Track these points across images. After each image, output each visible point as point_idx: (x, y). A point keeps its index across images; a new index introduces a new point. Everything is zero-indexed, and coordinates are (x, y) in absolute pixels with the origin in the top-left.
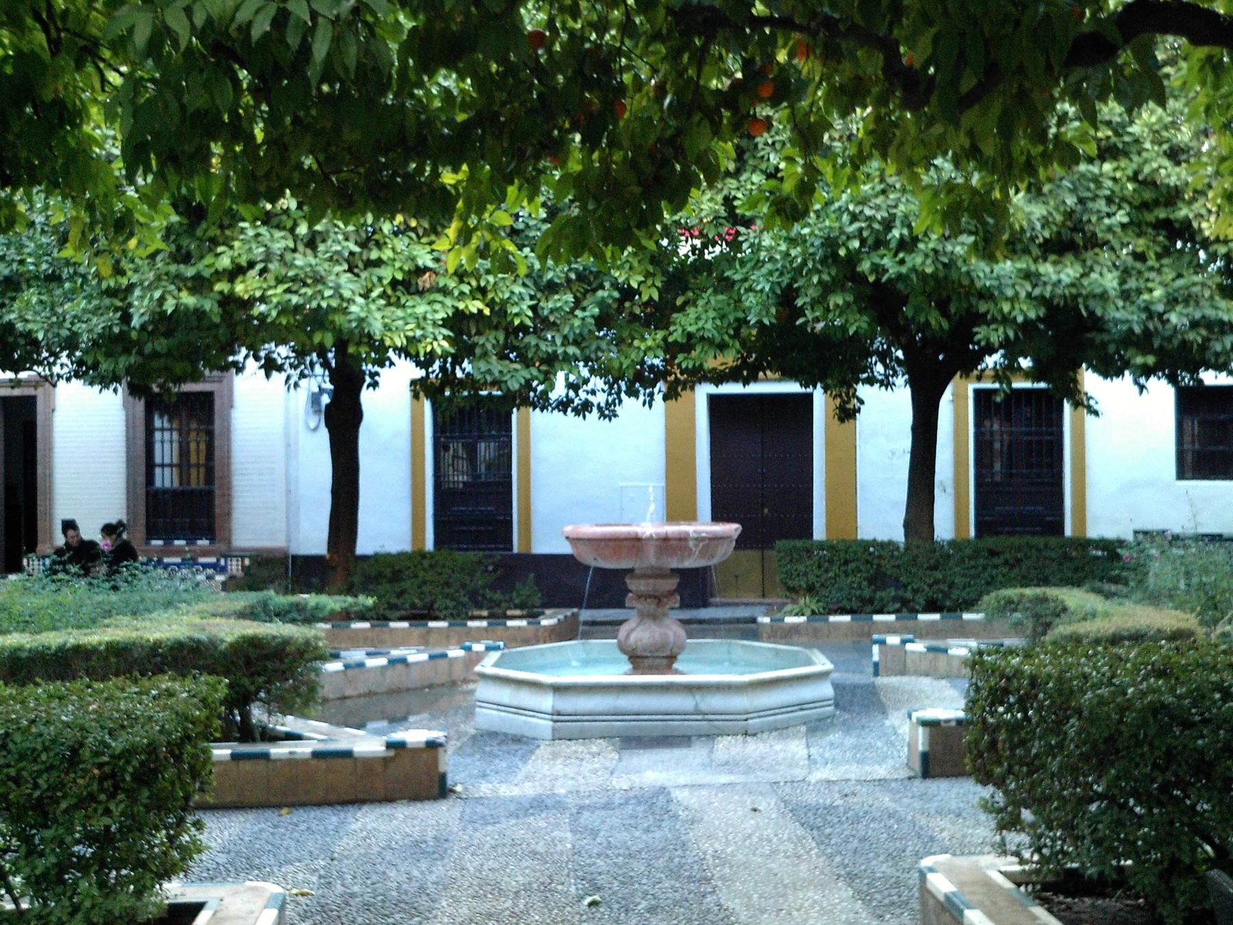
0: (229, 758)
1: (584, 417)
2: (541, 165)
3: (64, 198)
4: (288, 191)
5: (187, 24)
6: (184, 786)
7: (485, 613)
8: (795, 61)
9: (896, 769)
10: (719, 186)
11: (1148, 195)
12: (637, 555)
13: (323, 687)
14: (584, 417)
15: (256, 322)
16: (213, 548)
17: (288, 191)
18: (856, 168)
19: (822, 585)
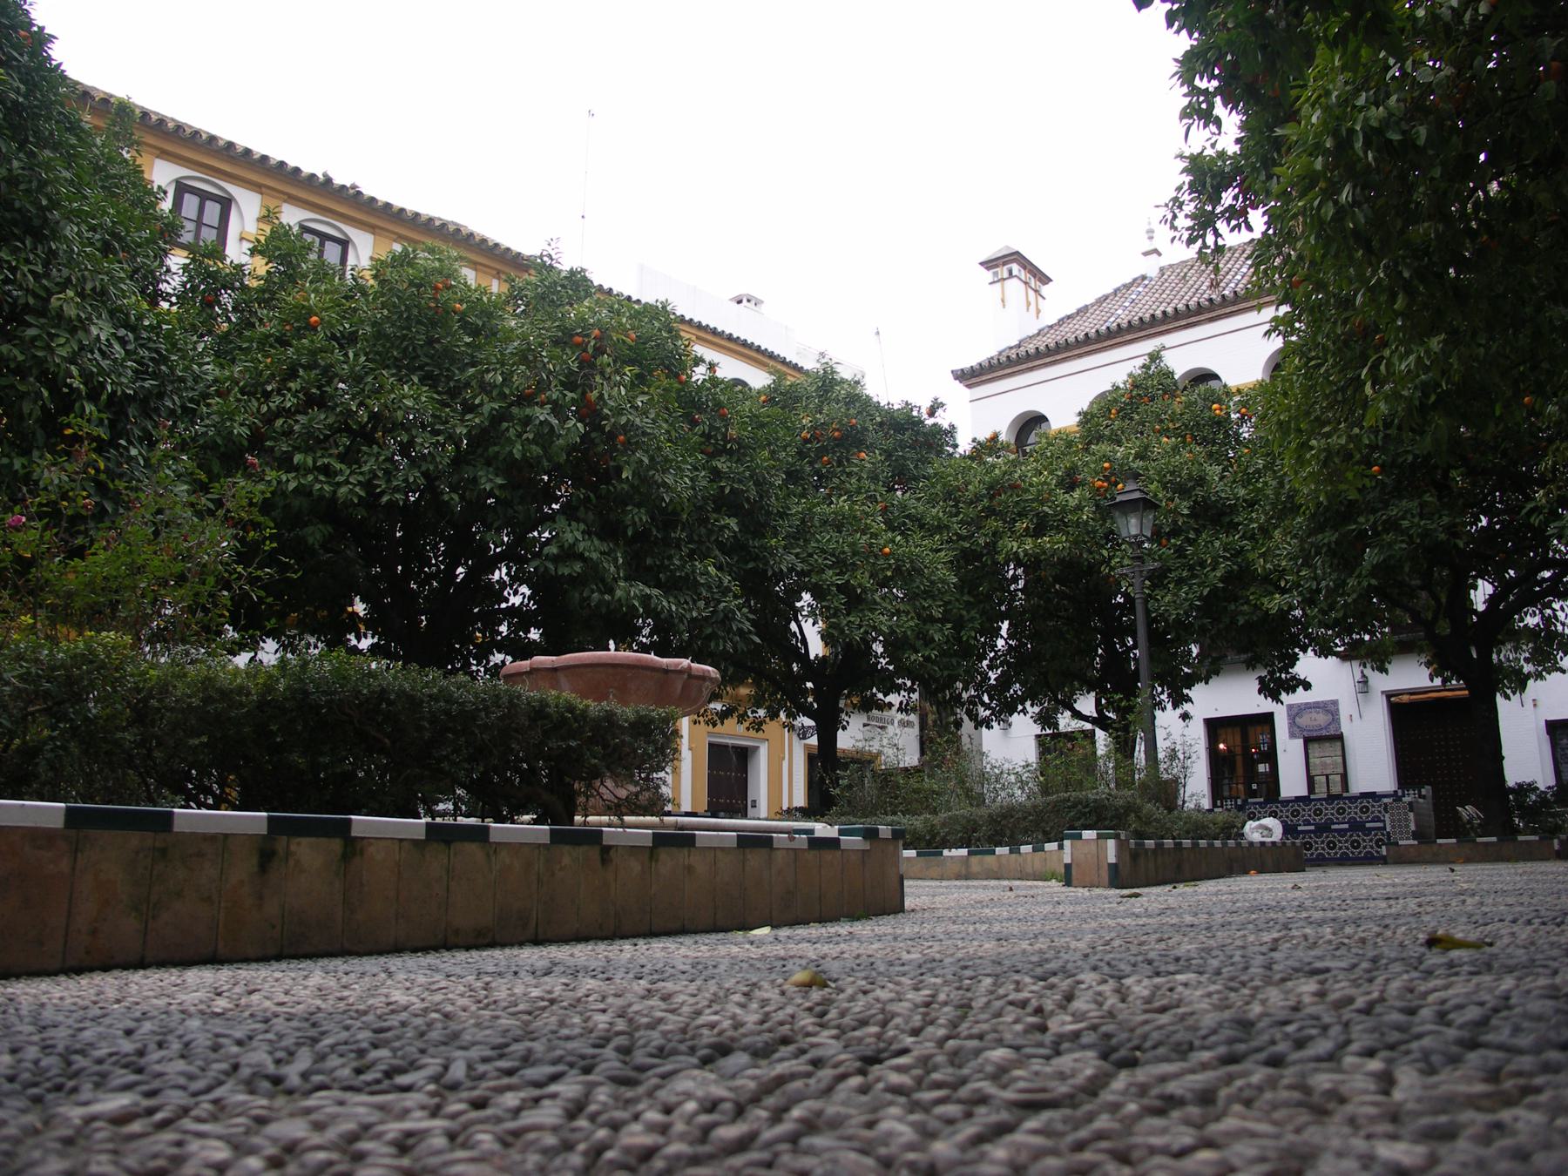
0: (58, 823)
1: (1176, 60)
2: (1220, 110)
3: (868, 705)
4: (611, 642)
5: (850, 1070)
6: (326, 292)
7: (793, 627)
8: (848, 739)
9: (251, 504)
10: (890, 752)
11: (1336, 926)
12: (857, 383)
13: (1130, 375)
14: (1176, 60)
15: (360, 608)
16: (1149, 346)
17: (611, 642)
18: (284, 381)
19: (793, 476)
